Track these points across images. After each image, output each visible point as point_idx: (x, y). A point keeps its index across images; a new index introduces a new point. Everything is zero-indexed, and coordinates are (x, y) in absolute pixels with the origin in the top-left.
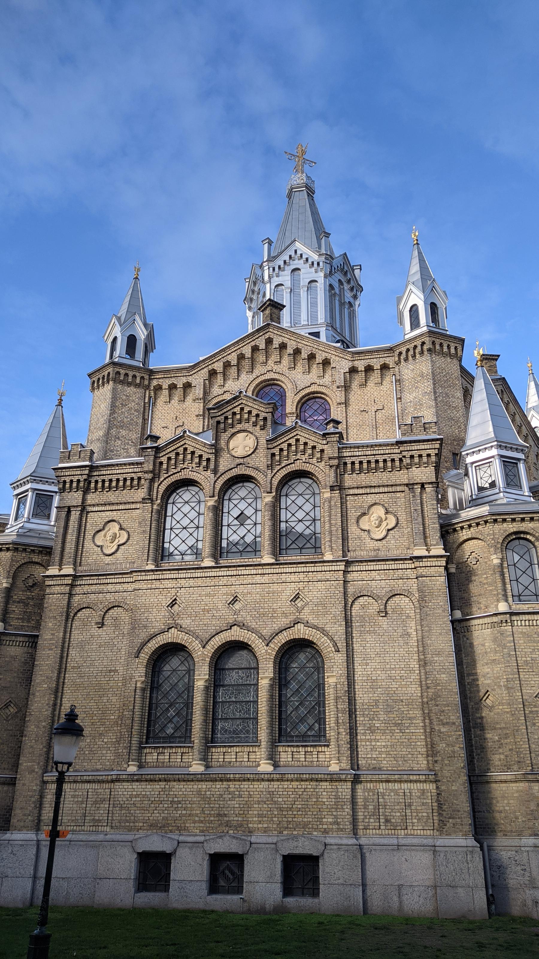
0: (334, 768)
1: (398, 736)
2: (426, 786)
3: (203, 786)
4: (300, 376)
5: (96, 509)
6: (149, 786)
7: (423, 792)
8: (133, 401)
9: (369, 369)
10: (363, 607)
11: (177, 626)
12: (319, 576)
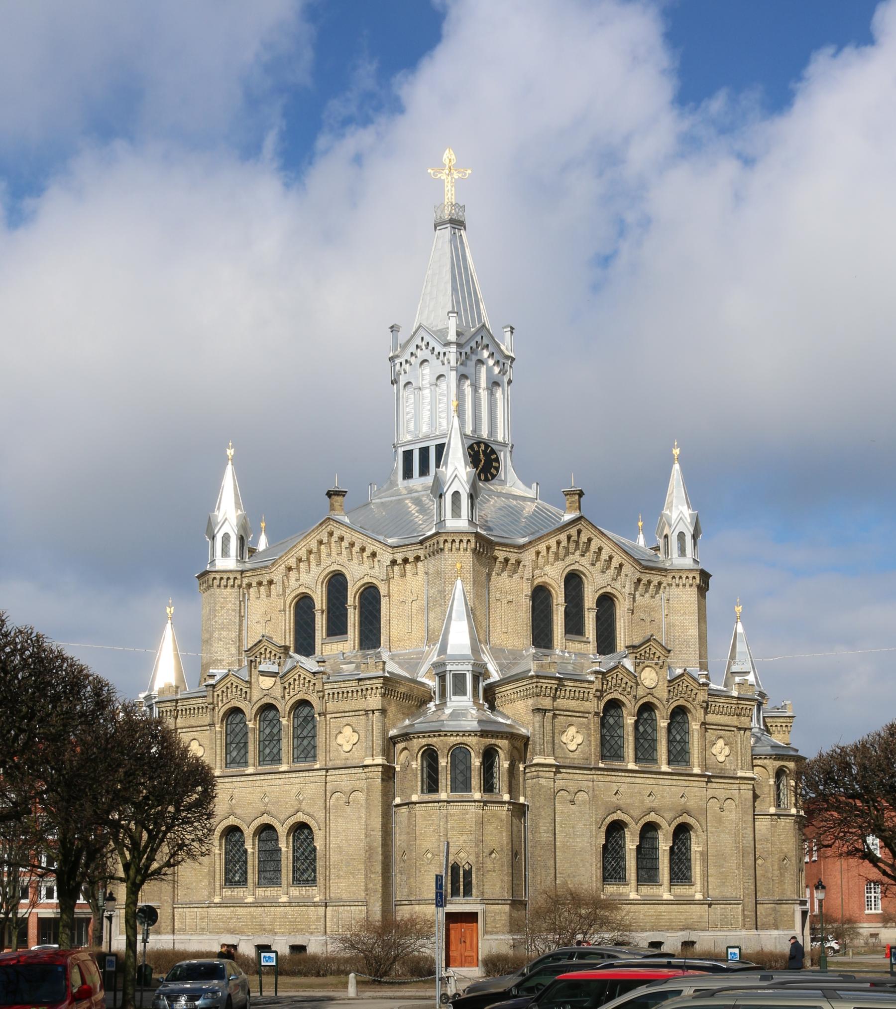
0: (317, 899)
1: (351, 880)
2: (362, 908)
3: (252, 909)
4: (356, 567)
5: (184, 730)
6: (226, 910)
7: (361, 911)
8: (230, 602)
9: (406, 561)
10: (337, 799)
11: (233, 814)
12: (312, 779)
